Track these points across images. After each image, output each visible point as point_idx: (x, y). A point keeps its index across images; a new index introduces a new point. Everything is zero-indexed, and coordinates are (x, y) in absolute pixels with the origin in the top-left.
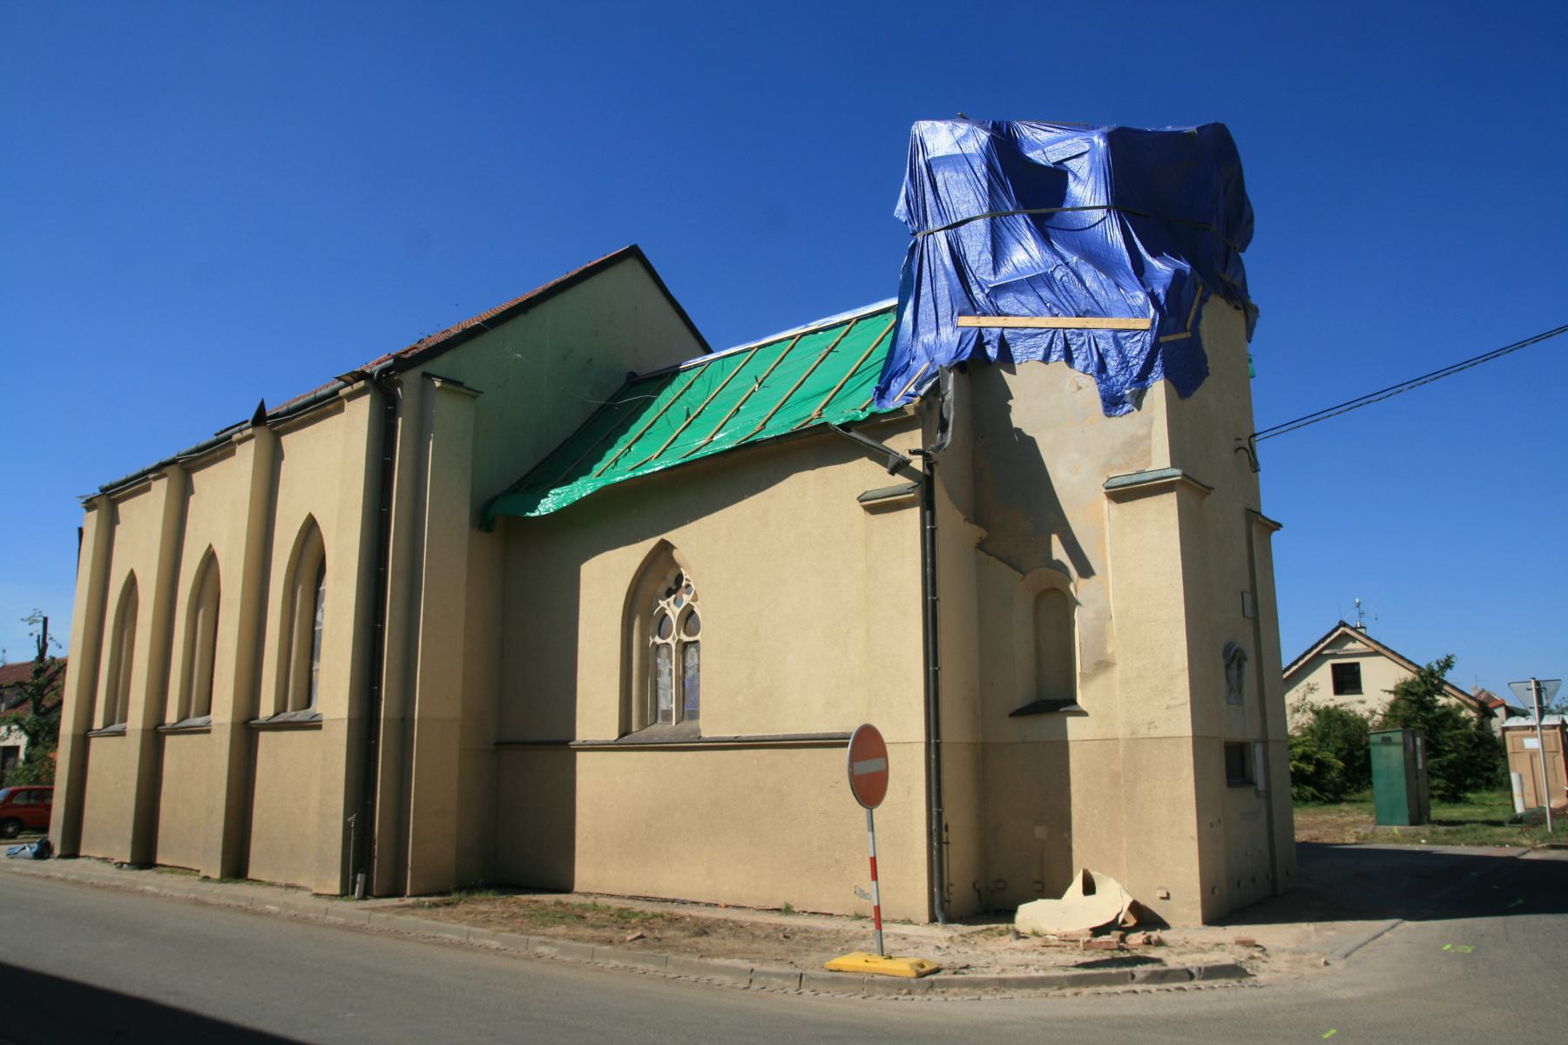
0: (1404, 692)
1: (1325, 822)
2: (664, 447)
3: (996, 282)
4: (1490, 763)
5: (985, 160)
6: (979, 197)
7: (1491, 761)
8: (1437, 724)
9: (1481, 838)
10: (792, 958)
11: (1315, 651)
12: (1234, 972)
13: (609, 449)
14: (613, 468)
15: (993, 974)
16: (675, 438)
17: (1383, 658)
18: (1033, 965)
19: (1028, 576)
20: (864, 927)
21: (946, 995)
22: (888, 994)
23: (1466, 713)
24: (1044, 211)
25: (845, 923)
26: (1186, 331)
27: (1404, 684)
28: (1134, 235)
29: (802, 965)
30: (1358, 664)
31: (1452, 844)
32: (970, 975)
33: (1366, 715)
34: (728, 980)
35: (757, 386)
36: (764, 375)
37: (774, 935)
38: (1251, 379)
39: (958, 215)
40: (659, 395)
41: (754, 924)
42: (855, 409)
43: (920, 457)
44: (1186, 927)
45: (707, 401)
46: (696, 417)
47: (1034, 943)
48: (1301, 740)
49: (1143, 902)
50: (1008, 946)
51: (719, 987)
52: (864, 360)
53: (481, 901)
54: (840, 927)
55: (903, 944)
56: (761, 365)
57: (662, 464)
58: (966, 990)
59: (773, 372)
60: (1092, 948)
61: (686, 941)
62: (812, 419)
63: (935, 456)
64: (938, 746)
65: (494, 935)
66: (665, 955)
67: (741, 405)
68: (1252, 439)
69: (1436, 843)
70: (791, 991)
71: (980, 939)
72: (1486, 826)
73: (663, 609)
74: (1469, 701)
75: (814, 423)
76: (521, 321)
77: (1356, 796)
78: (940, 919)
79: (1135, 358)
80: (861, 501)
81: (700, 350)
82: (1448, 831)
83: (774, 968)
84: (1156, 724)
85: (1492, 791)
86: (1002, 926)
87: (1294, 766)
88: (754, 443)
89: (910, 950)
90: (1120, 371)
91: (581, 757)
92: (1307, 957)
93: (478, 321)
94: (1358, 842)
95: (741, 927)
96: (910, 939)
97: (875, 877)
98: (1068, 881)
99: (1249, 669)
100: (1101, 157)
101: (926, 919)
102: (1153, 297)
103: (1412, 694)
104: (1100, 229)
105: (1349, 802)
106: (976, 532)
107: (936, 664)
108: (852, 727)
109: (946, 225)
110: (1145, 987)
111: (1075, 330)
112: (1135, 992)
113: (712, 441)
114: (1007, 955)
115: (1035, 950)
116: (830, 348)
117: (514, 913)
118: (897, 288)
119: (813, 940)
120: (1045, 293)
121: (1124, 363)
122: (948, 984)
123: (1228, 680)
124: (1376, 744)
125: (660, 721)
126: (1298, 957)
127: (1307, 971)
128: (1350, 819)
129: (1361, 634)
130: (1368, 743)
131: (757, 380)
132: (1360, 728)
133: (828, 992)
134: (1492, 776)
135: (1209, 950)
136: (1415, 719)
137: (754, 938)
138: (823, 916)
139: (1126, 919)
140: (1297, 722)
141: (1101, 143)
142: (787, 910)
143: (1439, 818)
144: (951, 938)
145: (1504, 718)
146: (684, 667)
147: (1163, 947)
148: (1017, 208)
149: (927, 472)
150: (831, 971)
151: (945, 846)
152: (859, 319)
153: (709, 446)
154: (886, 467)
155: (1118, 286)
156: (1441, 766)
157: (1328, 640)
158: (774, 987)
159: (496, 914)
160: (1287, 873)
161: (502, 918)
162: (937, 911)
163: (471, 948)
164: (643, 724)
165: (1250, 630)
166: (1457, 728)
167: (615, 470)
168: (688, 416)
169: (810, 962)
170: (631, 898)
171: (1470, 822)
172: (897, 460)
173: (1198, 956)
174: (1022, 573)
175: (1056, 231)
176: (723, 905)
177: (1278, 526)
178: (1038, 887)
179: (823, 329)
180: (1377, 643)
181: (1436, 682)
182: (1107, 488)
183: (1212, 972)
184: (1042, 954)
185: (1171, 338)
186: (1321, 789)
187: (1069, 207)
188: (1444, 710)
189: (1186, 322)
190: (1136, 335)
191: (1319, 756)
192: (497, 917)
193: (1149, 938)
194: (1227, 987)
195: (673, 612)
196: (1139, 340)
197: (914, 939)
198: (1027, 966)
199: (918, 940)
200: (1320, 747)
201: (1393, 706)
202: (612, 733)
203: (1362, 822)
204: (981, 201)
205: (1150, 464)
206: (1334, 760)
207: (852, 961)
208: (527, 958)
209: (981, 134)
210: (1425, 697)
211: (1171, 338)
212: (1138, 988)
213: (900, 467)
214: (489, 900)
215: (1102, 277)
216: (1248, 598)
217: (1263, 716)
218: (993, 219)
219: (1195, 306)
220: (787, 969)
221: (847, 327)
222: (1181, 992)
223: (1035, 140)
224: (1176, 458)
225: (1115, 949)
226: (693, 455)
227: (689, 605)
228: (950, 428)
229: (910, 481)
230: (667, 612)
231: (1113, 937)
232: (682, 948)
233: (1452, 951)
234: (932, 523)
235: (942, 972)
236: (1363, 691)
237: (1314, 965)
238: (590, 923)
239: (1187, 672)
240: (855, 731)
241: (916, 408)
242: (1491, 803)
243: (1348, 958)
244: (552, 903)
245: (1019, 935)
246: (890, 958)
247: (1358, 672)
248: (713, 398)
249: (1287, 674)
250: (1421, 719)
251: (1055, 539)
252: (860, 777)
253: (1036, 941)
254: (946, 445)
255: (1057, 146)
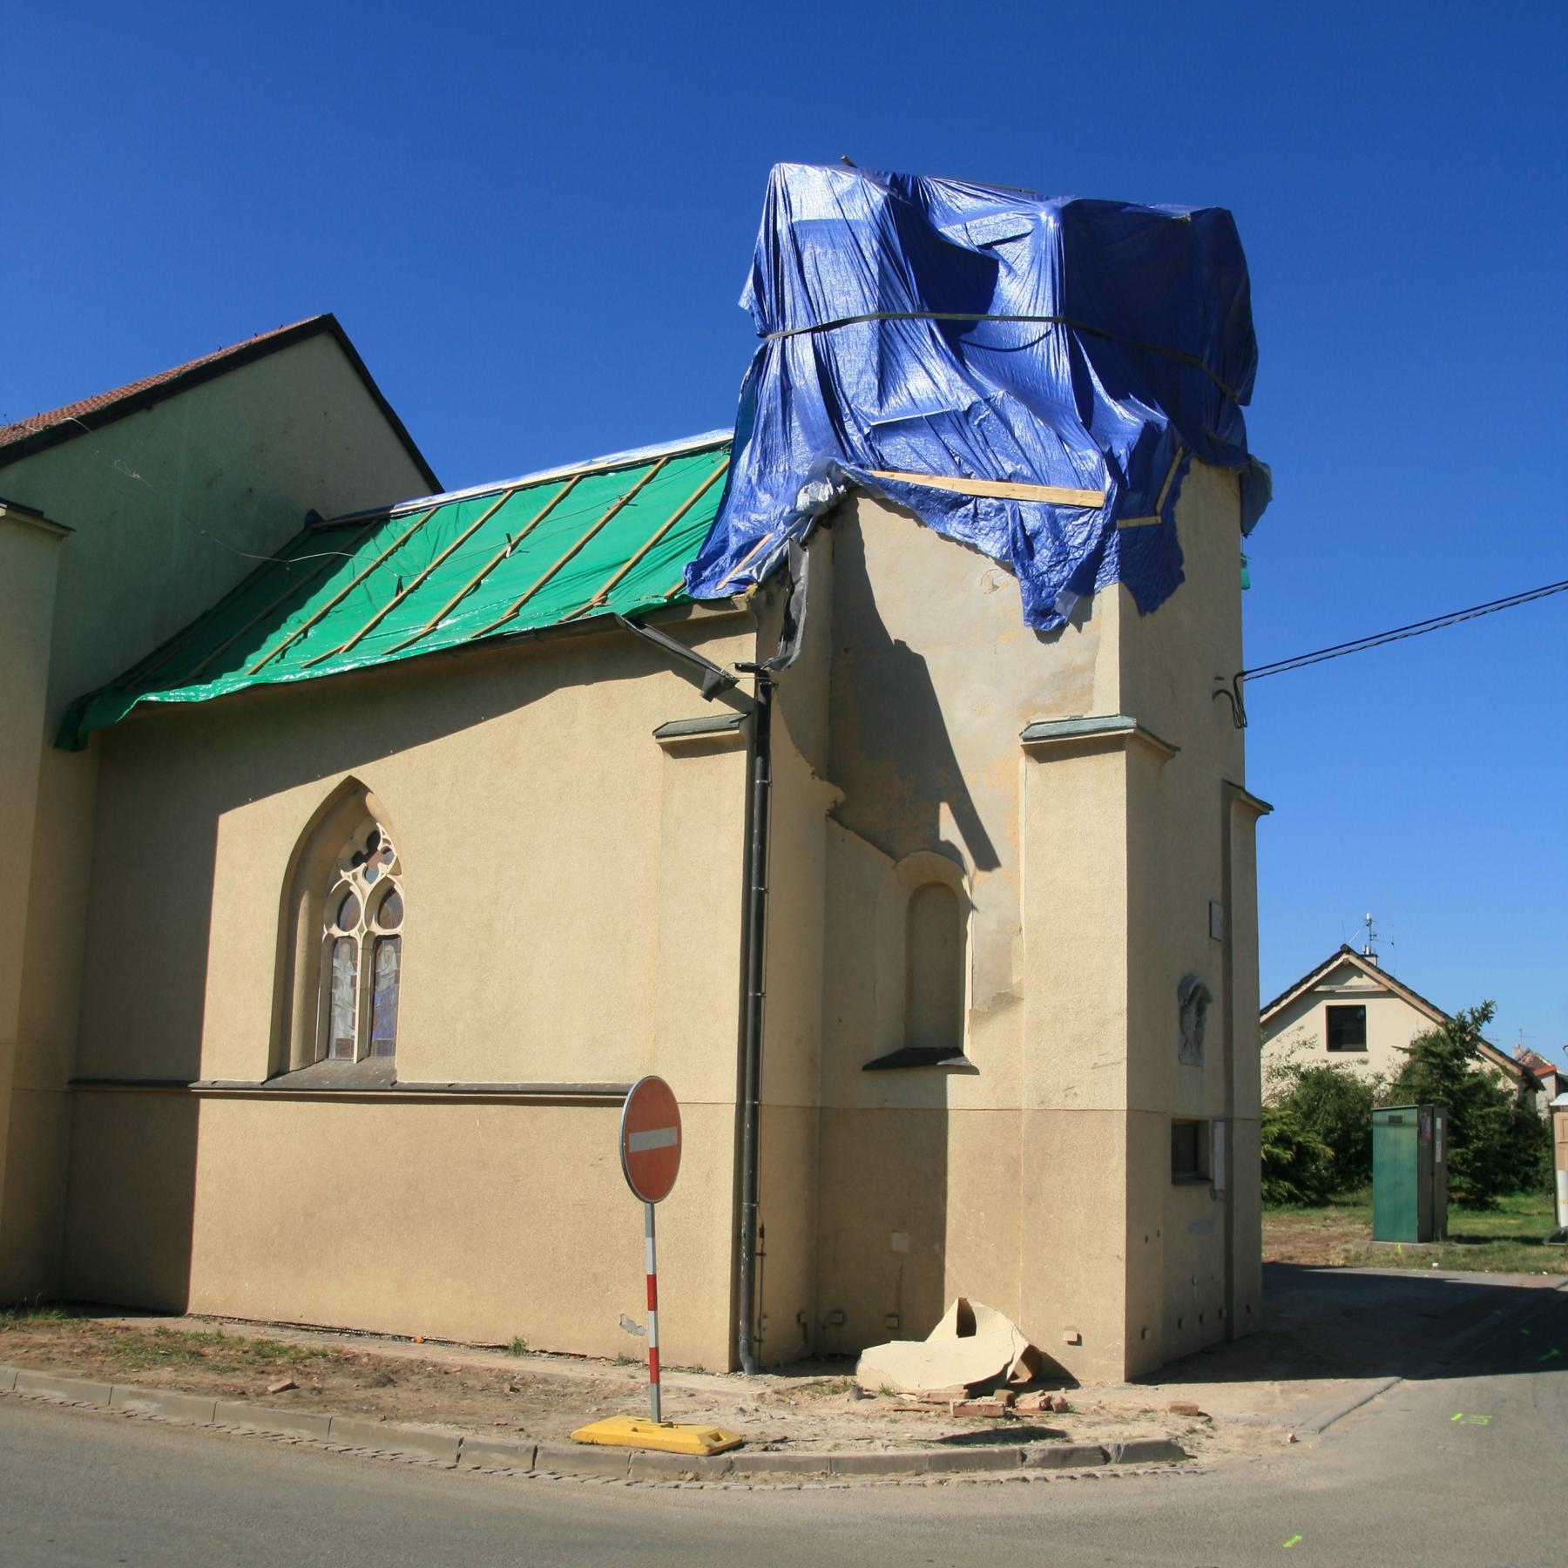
0: (1423, 1050)
1: (1304, 1233)
2: (360, 634)
3: (881, 418)
4: (1532, 1156)
5: (877, 231)
6: (866, 290)
7: (1531, 1151)
8: (1464, 1098)
9: (1512, 1261)
10: (521, 1423)
11: (1304, 987)
12: (1167, 1451)
13: (273, 632)
14: (277, 661)
15: (821, 1451)
16: (378, 621)
17: (1398, 1000)
18: (879, 1439)
19: (904, 861)
20: (632, 1377)
21: (750, 1481)
22: (665, 1480)
23: (1504, 1083)
24: (960, 317)
25: (606, 1370)
26: (1155, 514)
27: (1424, 1039)
28: (1089, 365)
29: (538, 1434)
30: (1363, 1008)
31: (1473, 1270)
32: (788, 1452)
33: (1370, 1081)
34: (424, 1455)
35: (510, 549)
36: (521, 534)
37: (496, 1386)
38: (1243, 591)
39: (831, 312)
40: (354, 553)
41: (465, 1370)
42: (657, 596)
43: (752, 675)
44: (1102, 1385)
45: (429, 568)
46: (411, 591)
47: (883, 1405)
48: (1278, 1114)
49: (1043, 1347)
50: (846, 1409)
51: (410, 1467)
52: (669, 527)
53: (37, 1328)
54: (596, 1376)
55: (690, 1404)
56: (516, 518)
57: (356, 661)
58: (780, 1474)
59: (534, 531)
60: (966, 1414)
61: (361, 1394)
62: (592, 607)
63: (775, 676)
64: (755, 1110)
65: (57, 1382)
66: (328, 1415)
67: (484, 576)
68: (1239, 678)
69: (1451, 1268)
70: (520, 1473)
71: (803, 1398)
72: (1520, 1245)
73: (347, 884)
74: (1509, 1066)
75: (593, 613)
76: (142, 420)
77: (1348, 1197)
78: (746, 1366)
79: (1078, 548)
80: (658, 737)
81: (420, 482)
82: (1469, 1251)
83: (494, 1437)
84: (1076, 1090)
85: (1529, 1195)
86: (838, 1379)
87: (1266, 1153)
88: (500, 638)
89: (698, 1414)
90: (1055, 565)
91: (209, 1110)
92: (1268, 1431)
93: (70, 414)
94: (1348, 1264)
95: (446, 1373)
96: (699, 1397)
97: (653, 1305)
98: (937, 1317)
99: (1214, 1013)
100: (1049, 244)
101: (726, 1366)
102: (1111, 460)
103: (1434, 1055)
104: (1040, 352)
105: (1337, 1204)
106: (829, 793)
107: (758, 987)
108: (631, 1076)
109: (812, 326)
110: (1039, 1472)
111: (994, 501)
112: (1025, 1480)
113: (435, 630)
114: (842, 1423)
115: (884, 1416)
116: (625, 498)
117: (91, 1347)
118: (734, 416)
119: (554, 1395)
120: (953, 440)
121: (1062, 553)
122: (753, 1465)
123: (1182, 1030)
124: (1381, 1124)
125: (333, 1055)
126: (1255, 1430)
127: (1269, 1451)
128: (1336, 1230)
129: (1369, 964)
130: (1369, 1122)
131: (510, 541)
132: (1362, 1100)
133: (575, 1475)
134: (1531, 1173)
135: (1133, 1420)
136: (1435, 1090)
137: (466, 1389)
138: (572, 1358)
139: (1018, 1373)
140: (1274, 1089)
141: (1051, 223)
142: (518, 1349)
143: (1458, 1232)
144: (762, 1395)
145: (1554, 1094)
146: (375, 975)
147: (1067, 1414)
148: (921, 308)
149: (761, 699)
150: (581, 1443)
151: (758, 1259)
152: (671, 457)
153: (430, 638)
154: (700, 688)
155: (1061, 439)
156: (1465, 1161)
157: (1325, 972)
158: (493, 1466)
159: (61, 1348)
160: (1248, 1307)
161: (72, 1354)
162: (742, 1355)
163: (20, 1402)
164: (308, 1060)
165: (1218, 955)
166: (1491, 1105)
167: (279, 665)
168: (400, 588)
169: (550, 1429)
170: (277, 1325)
171: (1499, 1238)
172: (716, 678)
173: (1117, 1429)
174: (892, 857)
175: (976, 348)
176: (419, 1338)
177: (1266, 808)
178: (893, 1322)
179: (616, 469)
180: (1391, 979)
181: (1468, 1039)
182: (1026, 739)
183: (1136, 1452)
184: (894, 1421)
185: (1133, 523)
186: (1301, 1185)
187: (997, 314)
188: (1474, 1080)
189: (1156, 502)
190: (1082, 515)
191: (1301, 1139)
192: (63, 1353)
193: (1048, 1400)
194: (1155, 1473)
195: (362, 889)
196: (1086, 523)
197: (705, 1396)
198: (871, 1439)
199: (713, 1397)
200: (1303, 1129)
201: (1408, 1071)
202: (257, 1072)
203: (1353, 1234)
204: (867, 294)
205: (1090, 707)
206: (1320, 1146)
207: (612, 1430)
208: (110, 1419)
209: (874, 192)
210: (1451, 1060)
211: (1133, 523)
212: (1030, 1474)
213: (720, 688)
214: (50, 1326)
215: (1039, 424)
216: (1218, 910)
217: (1229, 1082)
218: (882, 323)
219: (1170, 478)
220: (514, 1440)
221: (653, 468)
222: (1091, 1481)
223: (954, 208)
224: (1130, 700)
225: (999, 1417)
226: (409, 648)
227: (386, 879)
228: (799, 635)
229: (735, 711)
230: (351, 888)
231: (997, 1399)
232: (353, 1405)
233: (1463, 1422)
234: (765, 775)
235: (747, 1447)
236: (1368, 1047)
237: (1277, 1443)
238: (211, 1364)
239: (1125, 1016)
240: (636, 1083)
241: (750, 601)
242: (1526, 1212)
243: (1326, 1432)
244: (153, 1332)
245: (861, 1394)
246: (671, 1425)
247: (1364, 1018)
248: (438, 564)
249: (1264, 1018)
250: (1443, 1090)
251: (945, 810)
252: (638, 1155)
253: (886, 1403)
254: (792, 660)
255: (985, 221)
